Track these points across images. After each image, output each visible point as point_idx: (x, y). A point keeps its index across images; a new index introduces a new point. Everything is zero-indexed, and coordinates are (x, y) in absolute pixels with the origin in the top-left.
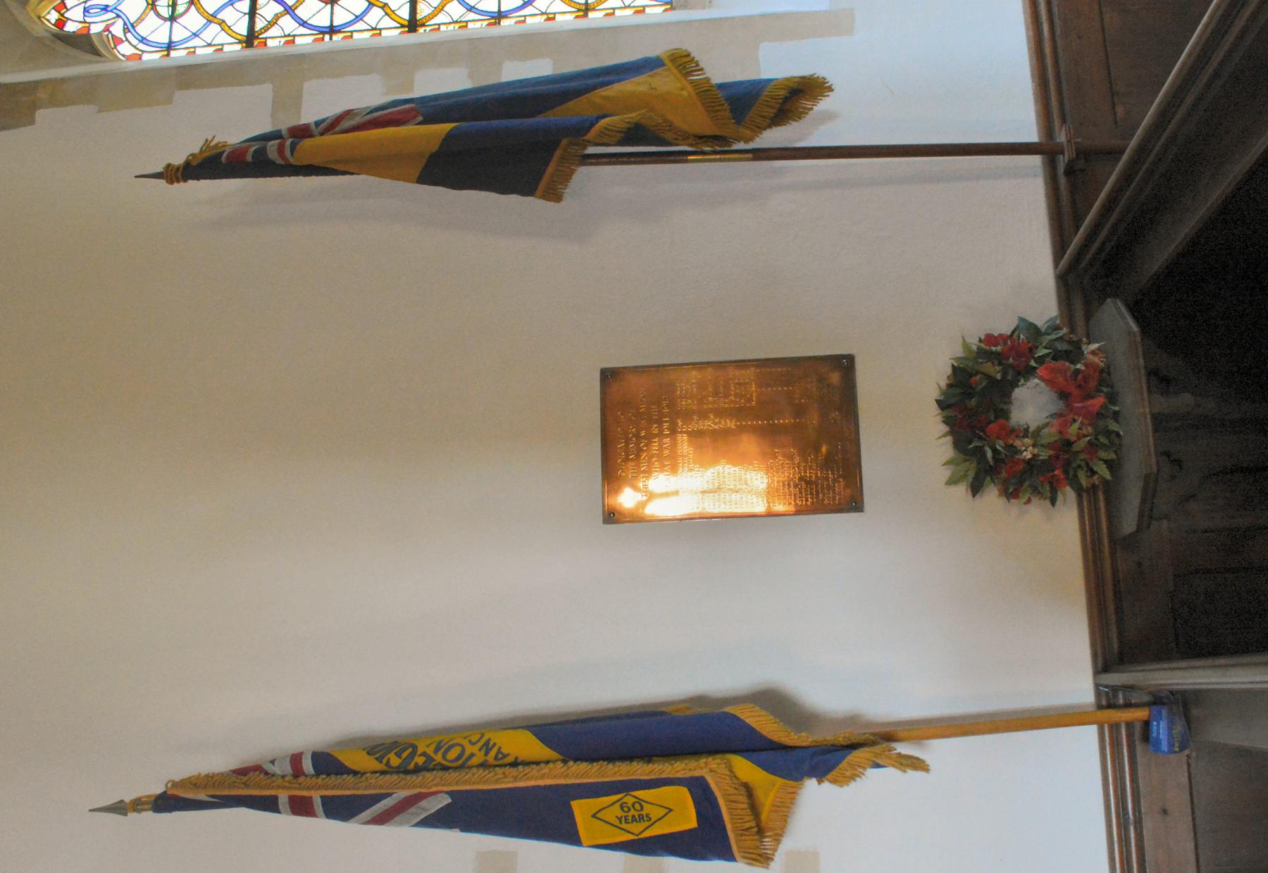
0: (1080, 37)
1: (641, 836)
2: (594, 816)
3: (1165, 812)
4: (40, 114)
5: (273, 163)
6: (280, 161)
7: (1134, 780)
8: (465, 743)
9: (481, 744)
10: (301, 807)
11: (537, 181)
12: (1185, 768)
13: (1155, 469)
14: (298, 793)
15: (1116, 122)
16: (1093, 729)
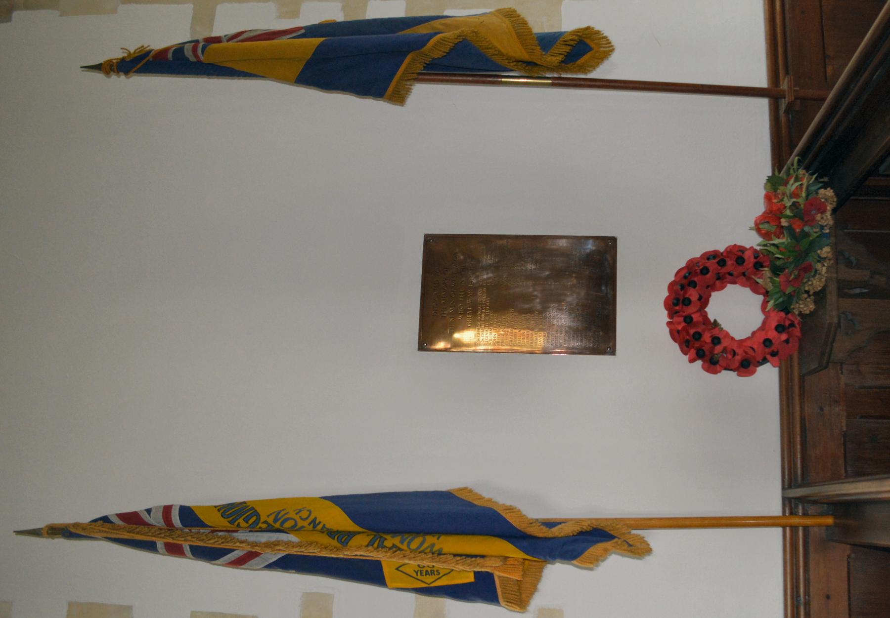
0: (803, 12)
1: (432, 585)
2: (397, 569)
3: (828, 597)
4: (15, 14)
5: (188, 59)
6: (192, 59)
7: (806, 571)
8: (298, 520)
9: (309, 520)
10: (174, 550)
11: (385, 90)
12: (846, 565)
13: (836, 320)
14: (171, 541)
15: (826, 78)
16: (779, 530)
